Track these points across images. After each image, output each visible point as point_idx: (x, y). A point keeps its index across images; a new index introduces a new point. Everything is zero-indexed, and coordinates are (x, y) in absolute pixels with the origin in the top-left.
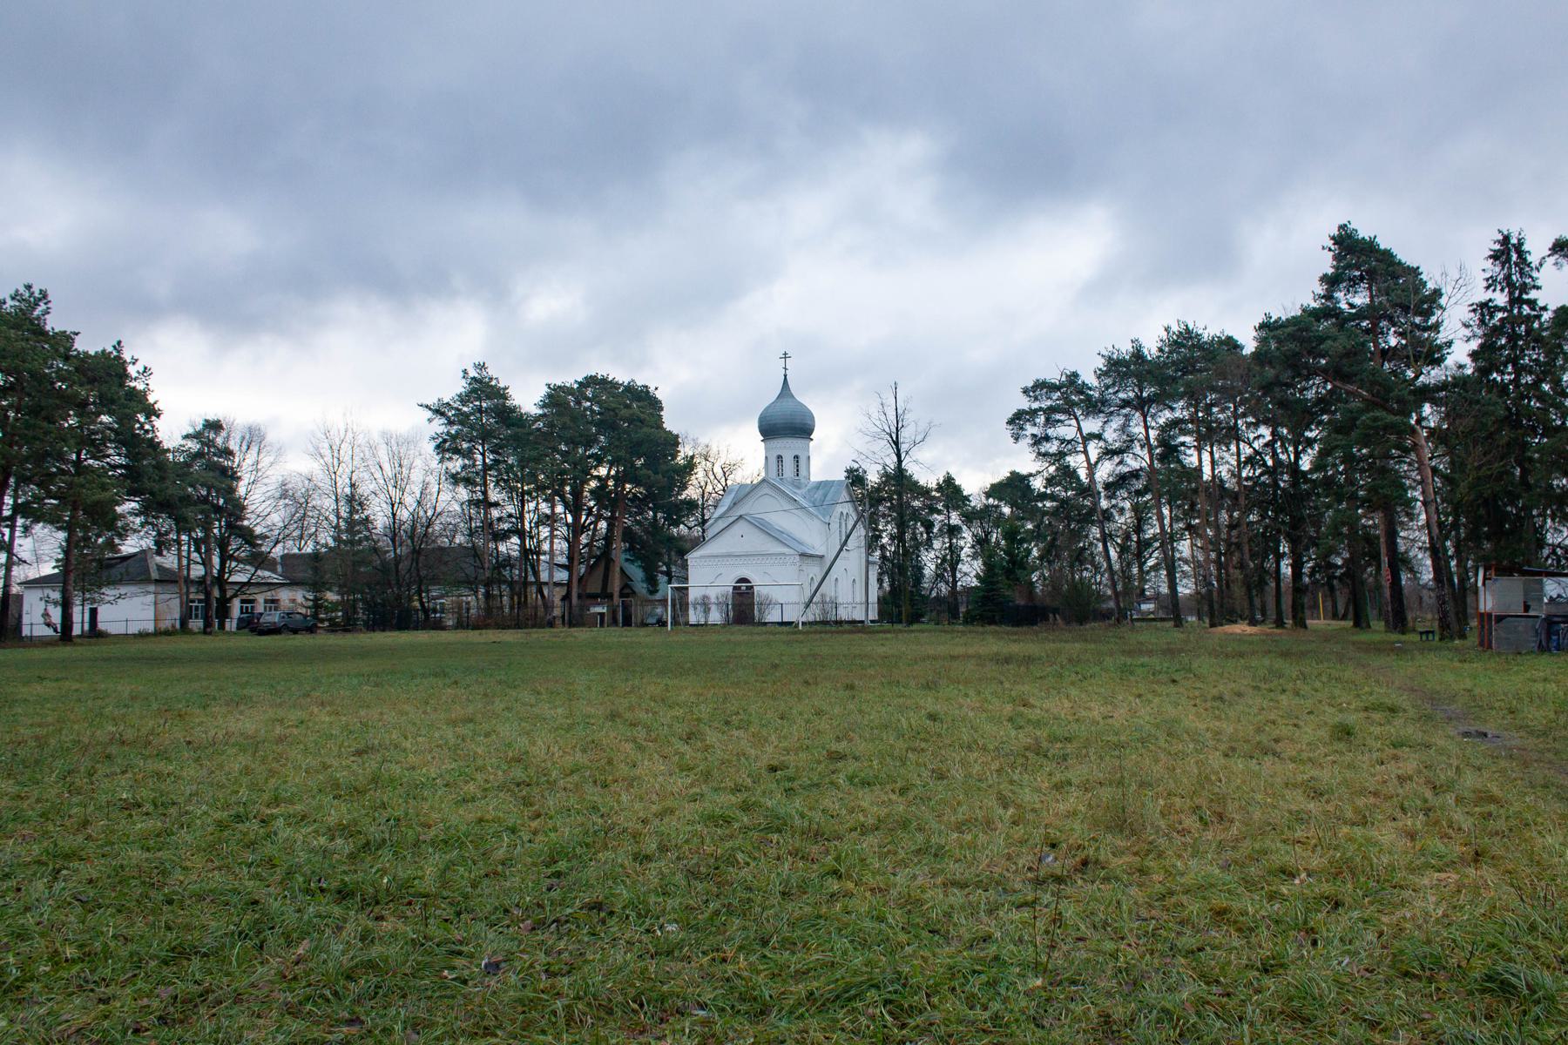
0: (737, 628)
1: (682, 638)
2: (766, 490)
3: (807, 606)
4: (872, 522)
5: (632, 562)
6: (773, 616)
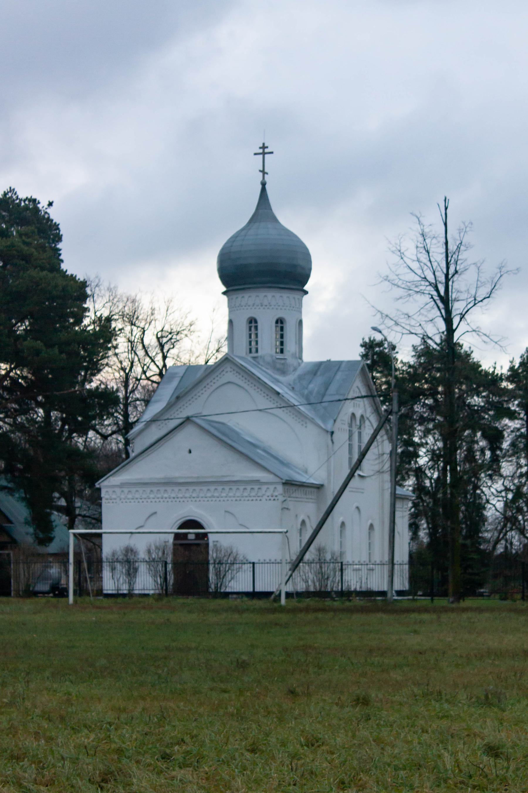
0: (181, 600)
1: (91, 617)
2: (229, 375)
3: (295, 566)
4: (404, 427)
5: (10, 491)
6: (240, 582)
